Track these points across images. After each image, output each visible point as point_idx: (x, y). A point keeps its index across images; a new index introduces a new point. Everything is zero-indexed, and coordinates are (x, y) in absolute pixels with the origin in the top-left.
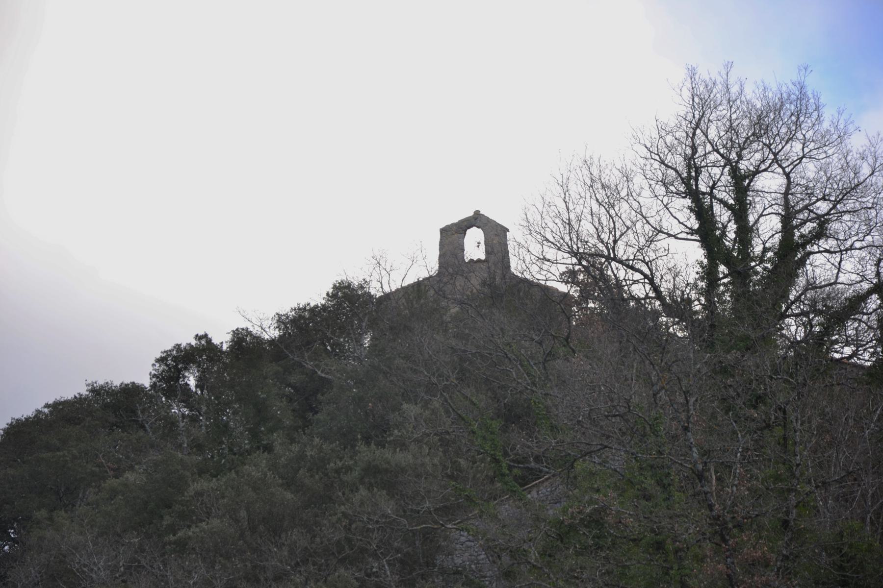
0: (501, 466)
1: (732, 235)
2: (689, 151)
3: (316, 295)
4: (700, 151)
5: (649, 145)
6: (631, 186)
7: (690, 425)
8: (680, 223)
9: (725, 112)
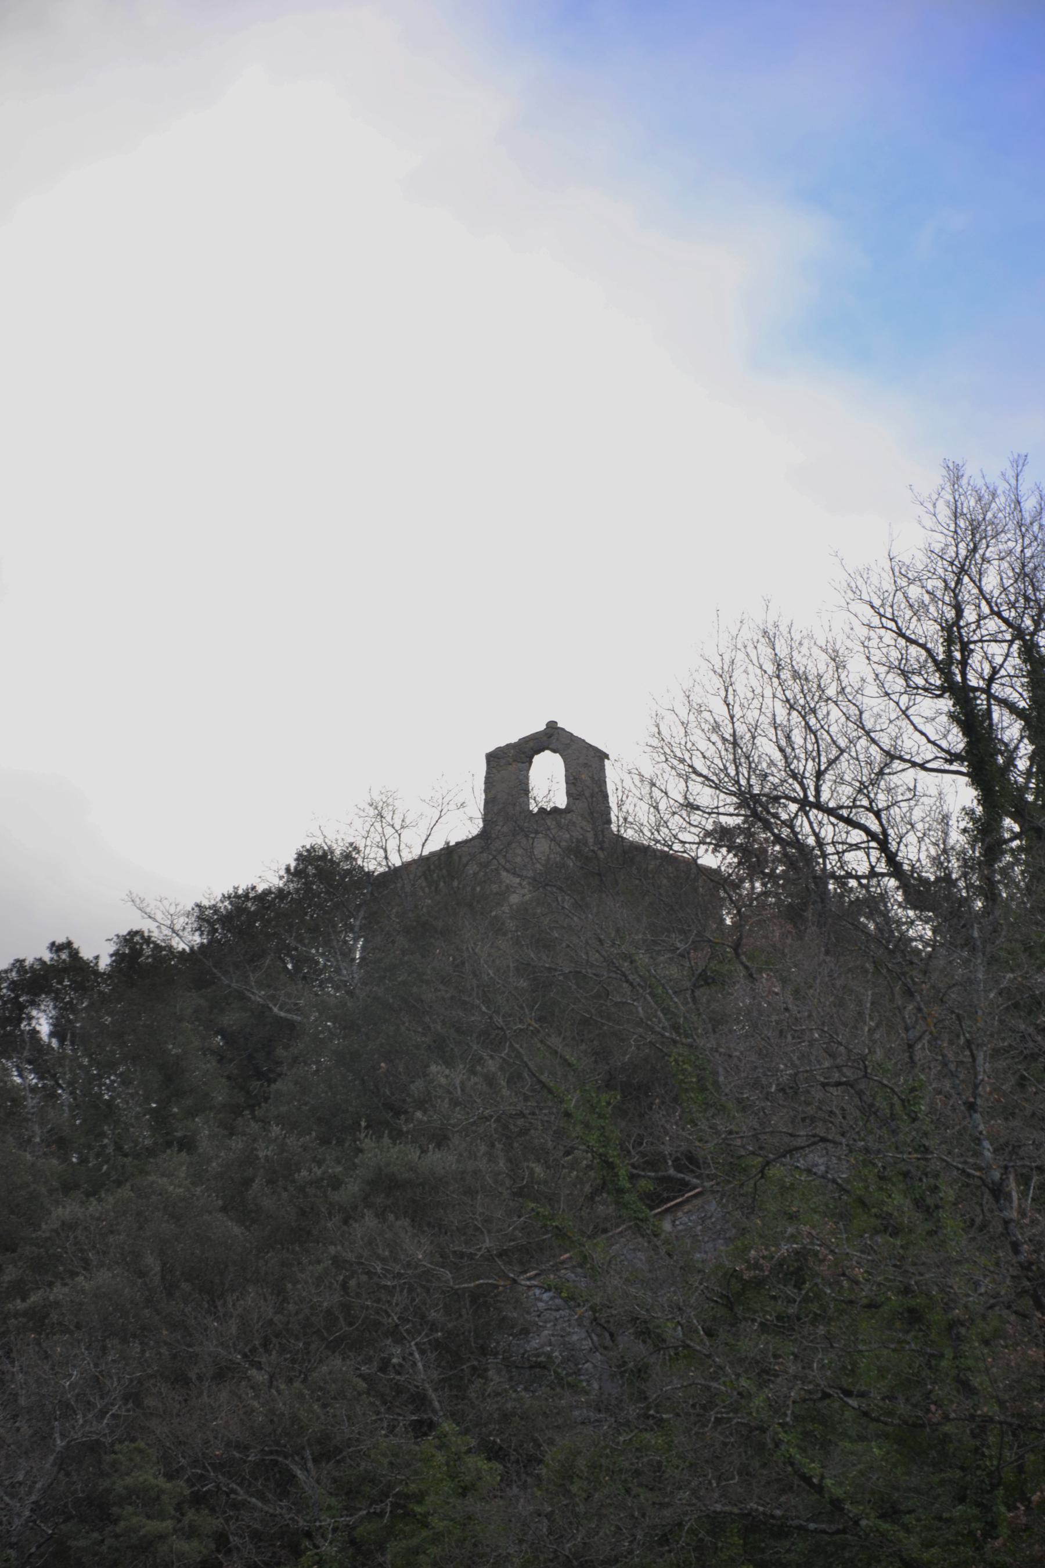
0: (616, 1175)
1: (1022, 764)
2: (950, 614)
3: (265, 868)
4: (970, 614)
5: (877, 603)
6: (842, 677)
7: (979, 1101)
8: (929, 741)
9: (1011, 544)
